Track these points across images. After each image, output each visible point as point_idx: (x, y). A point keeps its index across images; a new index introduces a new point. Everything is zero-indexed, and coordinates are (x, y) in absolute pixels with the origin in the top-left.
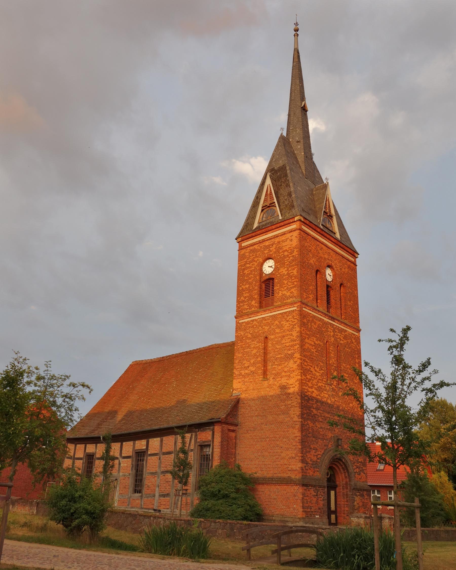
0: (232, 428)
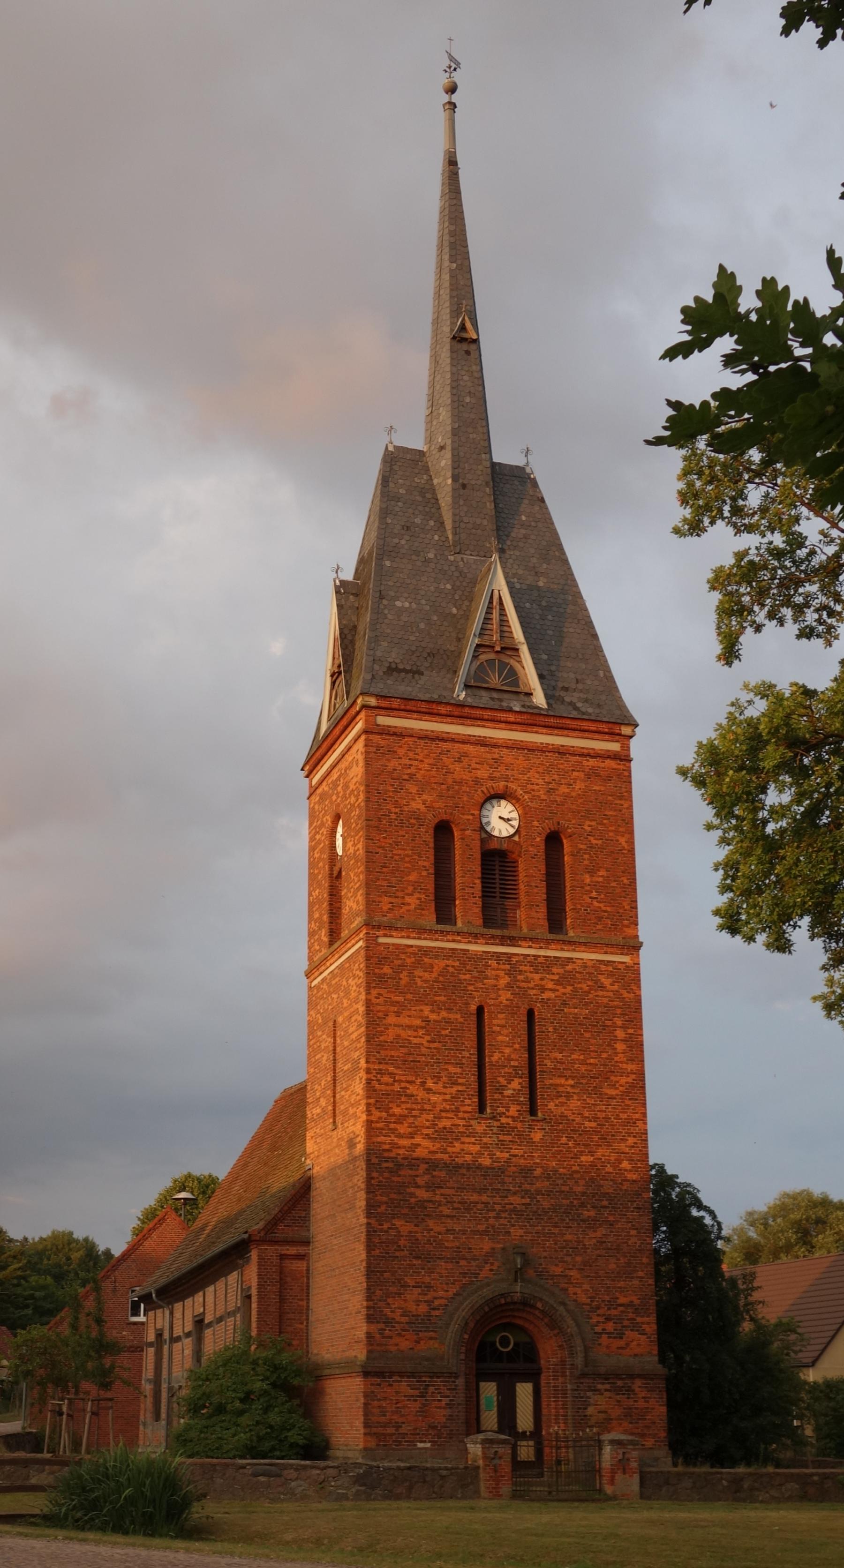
0: (292, 1250)
